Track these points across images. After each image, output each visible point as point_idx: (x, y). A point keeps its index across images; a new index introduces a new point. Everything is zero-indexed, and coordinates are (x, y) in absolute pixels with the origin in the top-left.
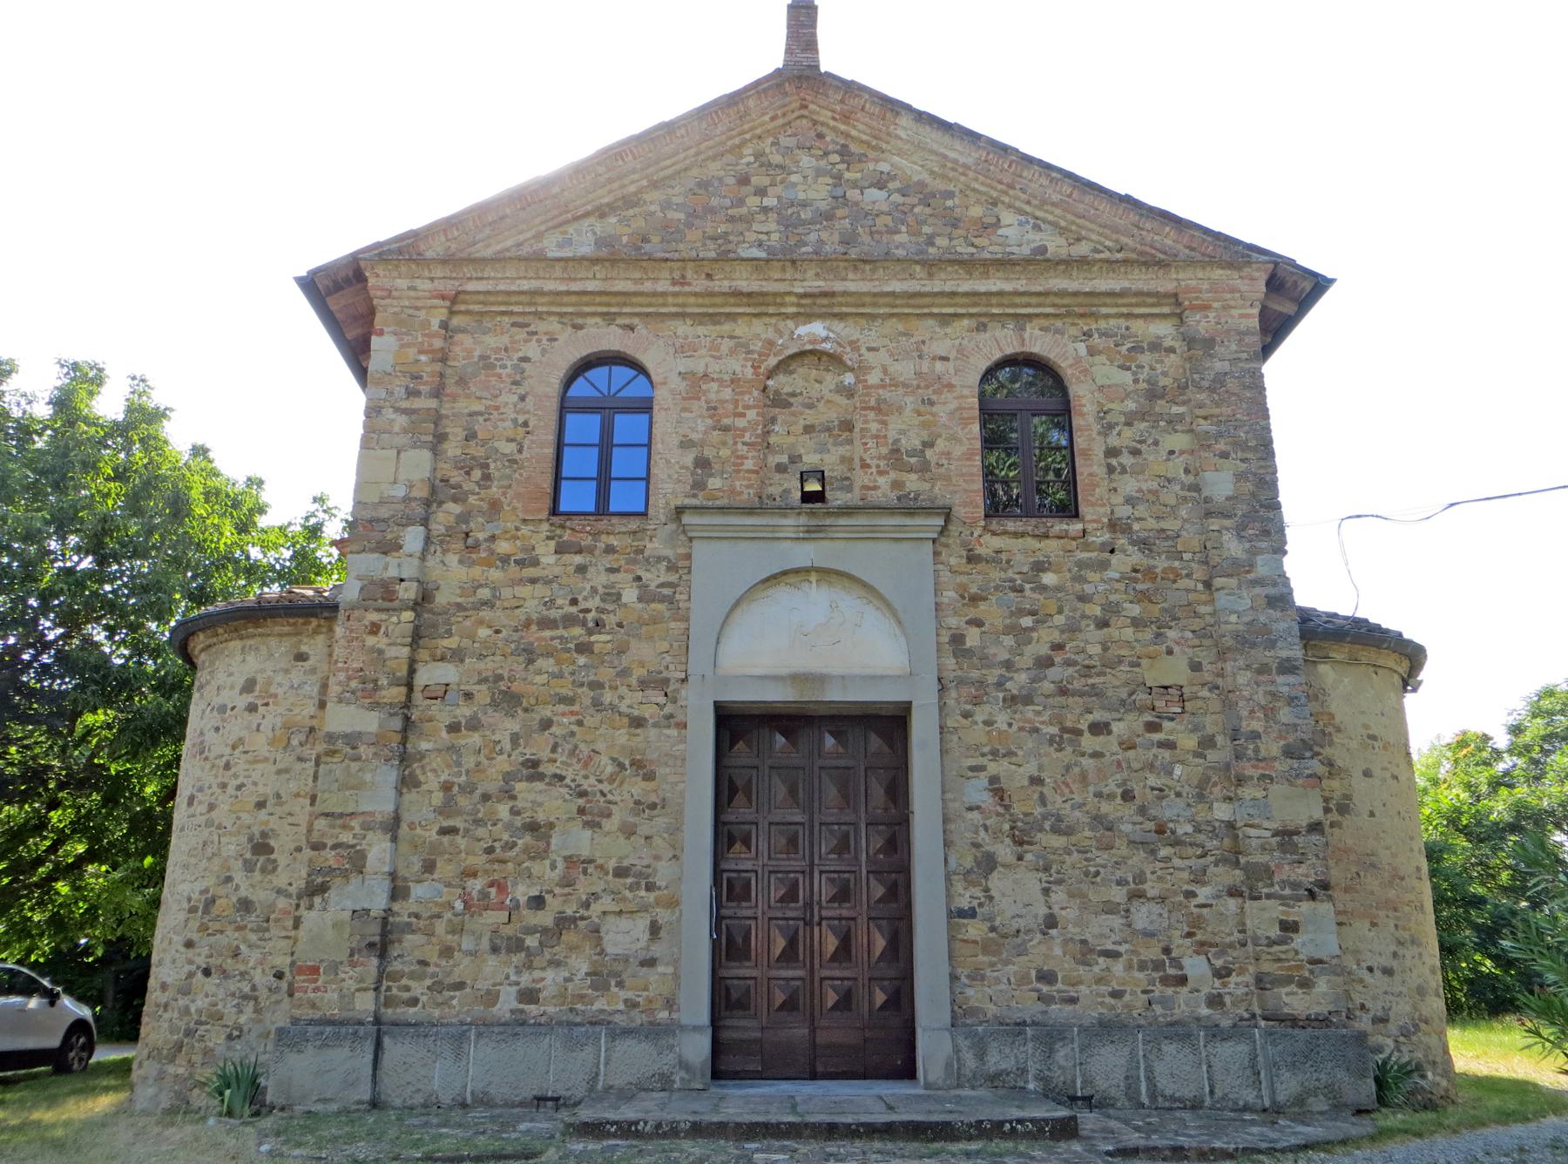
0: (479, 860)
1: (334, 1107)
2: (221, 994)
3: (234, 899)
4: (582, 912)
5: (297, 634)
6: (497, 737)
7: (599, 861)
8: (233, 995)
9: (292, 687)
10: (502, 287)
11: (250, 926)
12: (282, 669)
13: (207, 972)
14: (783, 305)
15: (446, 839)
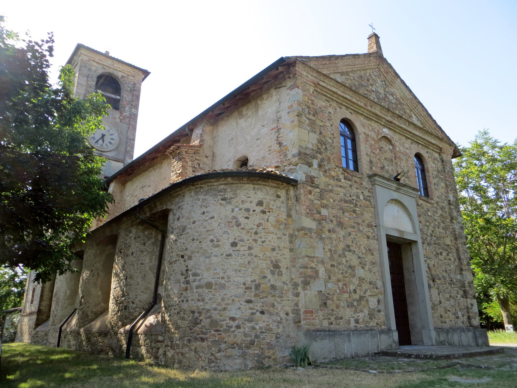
0: (340, 276)
1: (327, 360)
2: (271, 321)
3: (269, 285)
4: (364, 295)
5: (277, 188)
6: (339, 236)
7: (366, 279)
8: (275, 321)
9: (277, 207)
10: (328, 87)
11: (277, 295)
12: (272, 200)
13: (262, 313)
14: (381, 121)
15: (332, 268)
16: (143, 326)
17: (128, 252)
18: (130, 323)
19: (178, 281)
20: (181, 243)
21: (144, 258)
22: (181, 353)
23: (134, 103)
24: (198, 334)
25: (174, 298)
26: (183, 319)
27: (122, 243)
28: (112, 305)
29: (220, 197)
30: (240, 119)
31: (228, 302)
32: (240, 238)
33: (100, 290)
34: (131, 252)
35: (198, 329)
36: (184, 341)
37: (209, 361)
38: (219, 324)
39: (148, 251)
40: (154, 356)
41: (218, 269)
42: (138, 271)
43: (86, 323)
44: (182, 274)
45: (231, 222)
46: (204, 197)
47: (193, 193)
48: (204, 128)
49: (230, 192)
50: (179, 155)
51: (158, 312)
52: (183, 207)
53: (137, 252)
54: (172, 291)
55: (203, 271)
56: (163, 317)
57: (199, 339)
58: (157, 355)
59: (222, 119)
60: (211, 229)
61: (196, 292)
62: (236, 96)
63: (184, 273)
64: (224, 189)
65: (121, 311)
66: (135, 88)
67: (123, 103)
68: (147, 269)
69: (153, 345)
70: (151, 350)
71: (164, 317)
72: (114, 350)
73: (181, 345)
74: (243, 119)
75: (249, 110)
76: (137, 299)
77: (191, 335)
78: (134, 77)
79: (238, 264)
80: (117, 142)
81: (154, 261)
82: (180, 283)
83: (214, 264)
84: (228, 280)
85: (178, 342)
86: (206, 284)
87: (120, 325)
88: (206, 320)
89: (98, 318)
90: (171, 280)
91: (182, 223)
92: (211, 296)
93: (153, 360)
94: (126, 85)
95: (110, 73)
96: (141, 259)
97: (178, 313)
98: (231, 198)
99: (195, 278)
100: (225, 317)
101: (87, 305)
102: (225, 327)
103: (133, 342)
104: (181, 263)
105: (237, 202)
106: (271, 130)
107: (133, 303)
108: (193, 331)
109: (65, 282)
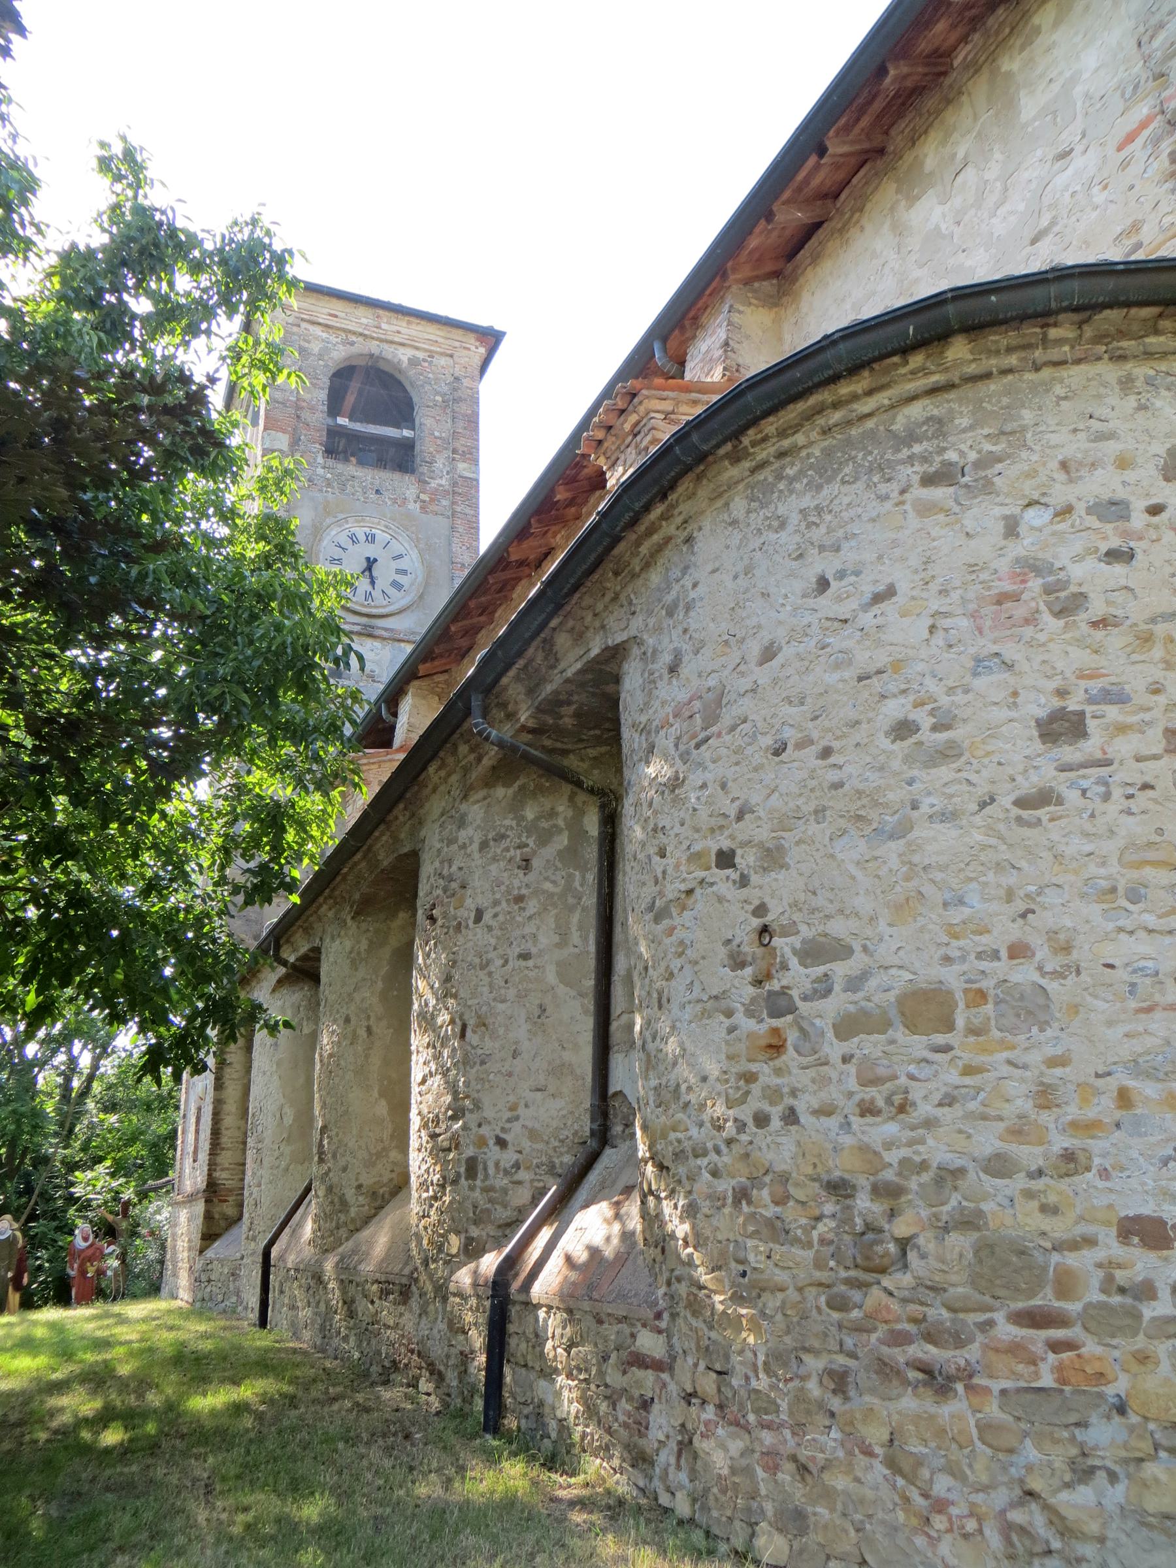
16: (555, 1263)
17: (462, 913)
18: (499, 1246)
19: (719, 1004)
20: (704, 786)
21: (529, 929)
22: (794, 1458)
23: (462, 441)
24: (899, 1339)
25: (703, 1106)
26: (776, 1230)
27: (432, 880)
28: (419, 1163)
29: (912, 473)
30: (912, 200)
31: (1091, 1113)
32: (1095, 686)
33: (382, 1094)
34: (473, 907)
35: (895, 1306)
36: (803, 1379)
37: (1009, 1542)
38: (1045, 1269)
39: (544, 892)
40: (627, 1447)
41: (974, 899)
42: (511, 993)
43: (343, 1232)
44: (738, 962)
45: (1015, 597)
46: (807, 501)
47: (739, 505)
48: (736, 318)
49: (971, 428)
50: (639, 438)
51: (620, 1185)
52: (692, 595)
53: (496, 903)
54: (691, 1065)
55: (873, 919)
56: (652, 1219)
57: (913, 1375)
58: (642, 1442)
59: (816, 259)
60: (882, 658)
61: (846, 1059)
62: (882, 71)
63: (750, 948)
64: (930, 419)
65: (455, 1182)
66: (459, 393)
67: (425, 447)
68: (551, 977)
69: (614, 1378)
70: (603, 1407)
71: (659, 1215)
72: (440, 1374)
73: (784, 1405)
74: (931, 192)
75: (956, 136)
76: (516, 1127)
77: (849, 1342)
78: (451, 356)
79: (1110, 847)
80: (420, 579)
81: (575, 938)
82: (729, 1014)
83: (943, 868)
84: (1062, 959)
85: (762, 1382)
86: (901, 1001)
87: (454, 1251)
88: (940, 1240)
89: (383, 1213)
90: (674, 1007)
91: (695, 683)
92: (953, 1077)
93: (622, 1471)
94: (427, 387)
95: (371, 356)
96: (518, 933)
97: (742, 1195)
98: (987, 461)
99: (820, 970)
100: (1082, 1218)
101: (342, 1162)
102: (1096, 1296)
103: (513, 1342)
104: (720, 899)
105: (1031, 474)
106: (1119, 149)
107: (502, 1143)
108: (855, 1314)
109: (275, 1077)
